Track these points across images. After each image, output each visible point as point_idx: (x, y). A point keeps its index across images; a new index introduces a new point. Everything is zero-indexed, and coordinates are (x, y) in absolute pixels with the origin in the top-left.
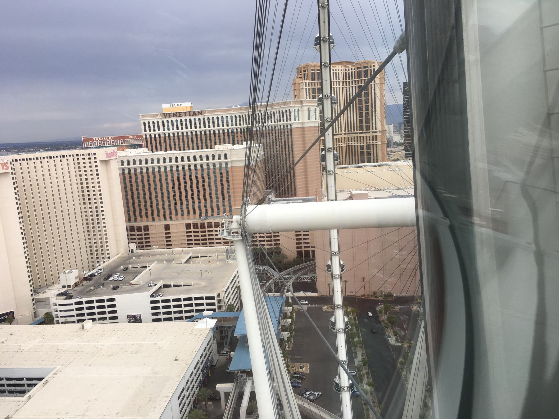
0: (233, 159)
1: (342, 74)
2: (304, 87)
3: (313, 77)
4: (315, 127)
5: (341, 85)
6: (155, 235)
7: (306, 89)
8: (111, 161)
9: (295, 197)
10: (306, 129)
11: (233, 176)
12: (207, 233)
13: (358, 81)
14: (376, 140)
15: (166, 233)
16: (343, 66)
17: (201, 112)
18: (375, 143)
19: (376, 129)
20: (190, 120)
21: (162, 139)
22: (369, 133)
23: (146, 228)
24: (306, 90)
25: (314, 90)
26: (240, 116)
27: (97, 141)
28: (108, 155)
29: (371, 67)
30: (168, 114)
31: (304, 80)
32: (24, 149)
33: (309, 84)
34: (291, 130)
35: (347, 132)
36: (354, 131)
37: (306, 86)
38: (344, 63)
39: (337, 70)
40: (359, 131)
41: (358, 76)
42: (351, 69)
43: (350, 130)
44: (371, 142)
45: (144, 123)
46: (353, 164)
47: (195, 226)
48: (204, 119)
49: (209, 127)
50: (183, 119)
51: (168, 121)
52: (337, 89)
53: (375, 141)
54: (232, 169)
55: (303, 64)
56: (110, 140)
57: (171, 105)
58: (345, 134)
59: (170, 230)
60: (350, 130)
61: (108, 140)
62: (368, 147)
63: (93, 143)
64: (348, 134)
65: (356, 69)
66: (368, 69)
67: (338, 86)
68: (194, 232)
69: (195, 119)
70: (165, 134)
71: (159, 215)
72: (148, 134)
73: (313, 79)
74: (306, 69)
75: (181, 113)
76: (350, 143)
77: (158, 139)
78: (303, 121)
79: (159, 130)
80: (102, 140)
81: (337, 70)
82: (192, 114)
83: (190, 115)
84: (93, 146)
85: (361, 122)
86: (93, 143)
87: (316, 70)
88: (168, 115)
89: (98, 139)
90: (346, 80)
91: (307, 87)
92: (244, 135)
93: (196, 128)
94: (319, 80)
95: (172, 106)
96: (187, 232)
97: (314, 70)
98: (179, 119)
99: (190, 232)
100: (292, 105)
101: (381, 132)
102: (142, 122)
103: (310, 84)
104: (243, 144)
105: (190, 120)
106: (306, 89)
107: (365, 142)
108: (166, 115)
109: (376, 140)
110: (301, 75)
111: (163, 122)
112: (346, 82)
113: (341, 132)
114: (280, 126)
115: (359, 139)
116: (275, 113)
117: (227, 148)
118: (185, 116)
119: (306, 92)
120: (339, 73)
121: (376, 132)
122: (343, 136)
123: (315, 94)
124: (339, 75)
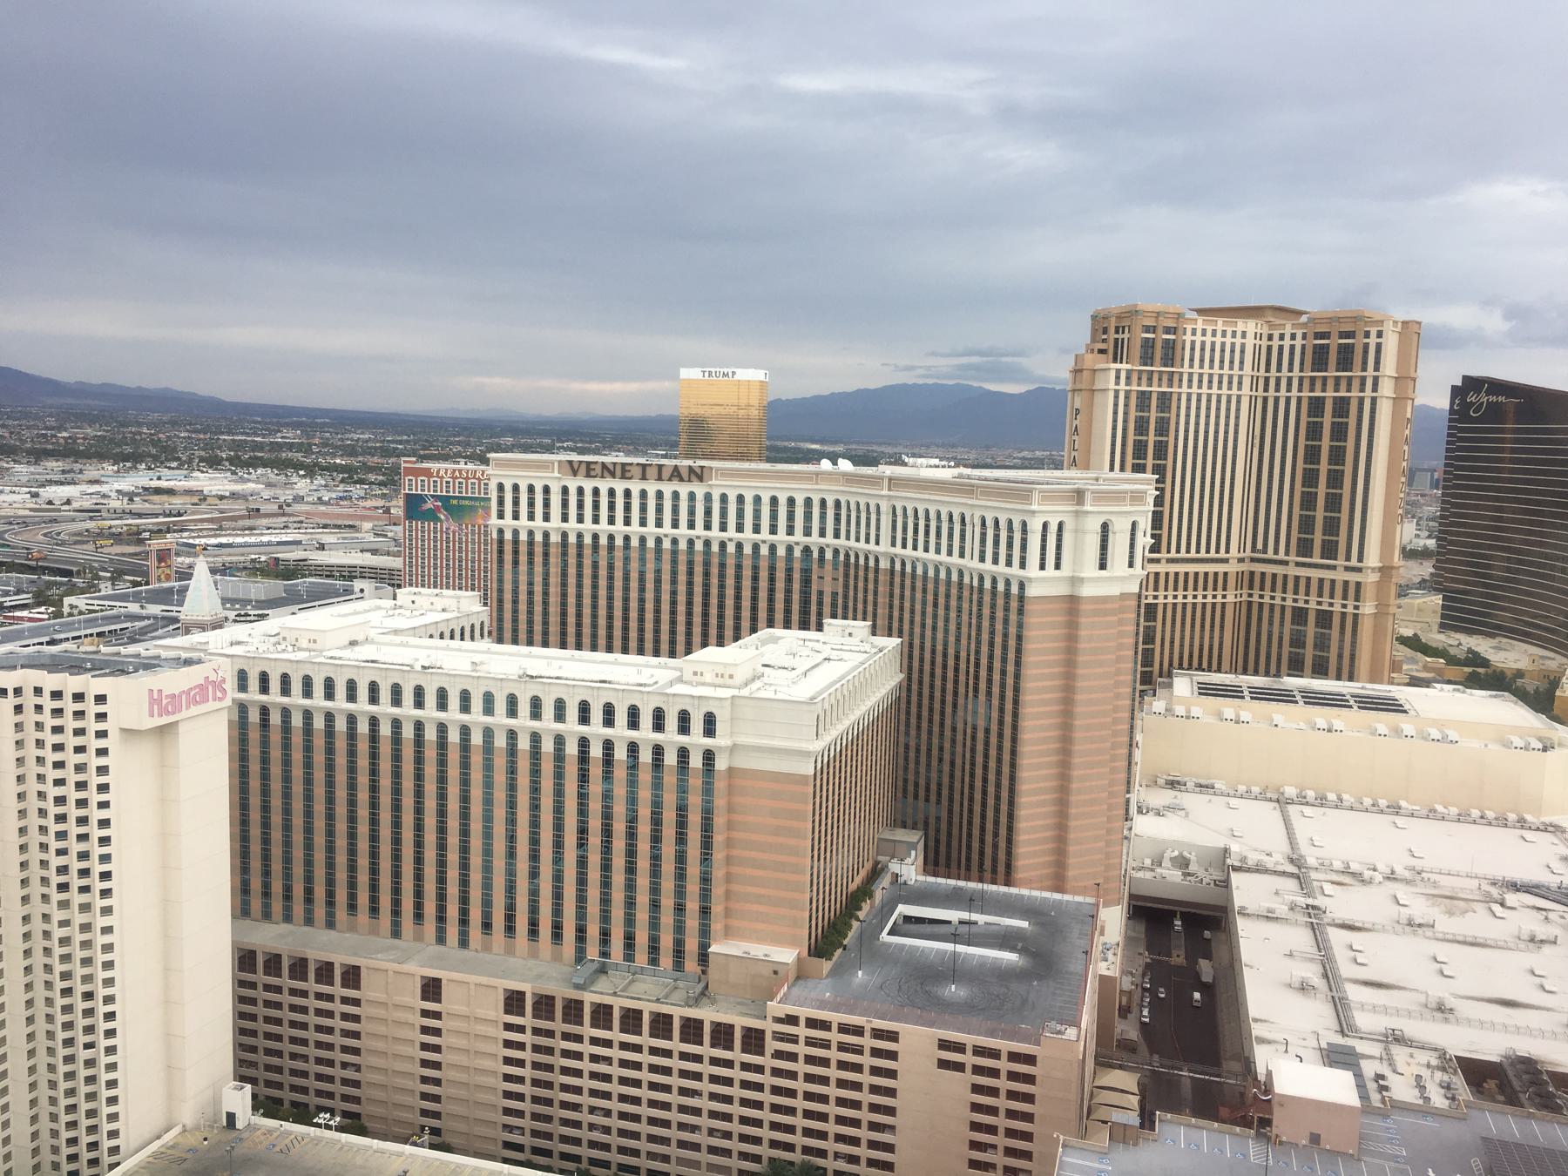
0: (742, 740)
1: (1257, 350)
2: (1112, 386)
3: (1146, 353)
4: (1124, 596)
5: (1246, 390)
6: (381, 1013)
7: (1117, 392)
8: (182, 728)
9: (1008, 883)
10: (1083, 607)
11: (730, 809)
12: (587, 1049)
13: (1313, 379)
14: (1357, 599)
15: (425, 1013)
16: (1260, 322)
17: (699, 471)
18: (1350, 609)
19: (1360, 560)
20: (660, 495)
21: (552, 550)
22: (1334, 568)
23: (352, 976)
24: (1116, 397)
25: (1144, 398)
26: (838, 504)
27: (443, 477)
28: (157, 702)
29: (1367, 335)
30: (583, 467)
31: (1115, 361)
32: (350, 432)
33: (1128, 378)
34: (1021, 598)
35: (1248, 552)
36: (1276, 552)
37: (1117, 383)
38: (1270, 312)
39: (1239, 335)
40: (1293, 558)
41: (1313, 364)
42: (1292, 336)
43: (1260, 546)
44: (1338, 602)
45: (501, 487)
46: (1256, 673)
47: (544, 1005)
48: (708, 497)
49: (723, 528)
50: (636, 487)
51: (580, 491)
52: (1229, 402)
53: (1351, 603)
54: (730, 777)
55: (1115, 304)
56: (479, 479)
57: (704, 372)
58: (1241, 560)
59: (439, 1001)
60: (1260, 546)
61: (474, 478)
62: (1324, 618)
63: (429, 481)
64: (1253, 560)
65: (1310, 336)
66: (1359, 342)
67: (1235, 391)
68: (536, 1032)
69: (676, 495)
70: (565, 535)
71: (419, 916)
72: (508, 526)
73: (1147, 359)
74: (1126, 323)
75: (628, 468)
76: (1256, 592)
77: (538, 550)
78: (1077, 574)
79: (546, 518)
80: (457, 478)
81: (1239, 335)
82: (666, 473)
83: (660, 478)
84: (429, 491)
85: (1307, 525)
86: (429, 481)
87: (1160, 330)
88: (583, 469)
89: (446, 473)
90: (1267, 370)
91: (1122, 386)
92: (846, 576)
93: (675, 525)
94: (1165, 366)
95: (707, 374)
96: (509, 1027)
97: (1153, 329)
98: (620, 486)
99: (521, 1029)
100: (1034, 507)
101: (1380, 569)
102: (493, 486)
103: (1135, 377)
104: (825, 627)
105: (660, 495)
106: (1117, 392)
107: (1313, 599)
108: (576, 467)
109: (1357, 599)
110: (1104, 341)
111: (565, 490)
112: (1267, 380)
113: (1227, 551)
114: (981, 578)
115: (1290, 585)
116: (968, 520)
117: (731, 677)
118: (644, 478)
119: (1116, 405)
120: (1243, 346)
121: (1359, 570)
122: (1232, 568)
123: (1145, 414)
124: (1242, 351)
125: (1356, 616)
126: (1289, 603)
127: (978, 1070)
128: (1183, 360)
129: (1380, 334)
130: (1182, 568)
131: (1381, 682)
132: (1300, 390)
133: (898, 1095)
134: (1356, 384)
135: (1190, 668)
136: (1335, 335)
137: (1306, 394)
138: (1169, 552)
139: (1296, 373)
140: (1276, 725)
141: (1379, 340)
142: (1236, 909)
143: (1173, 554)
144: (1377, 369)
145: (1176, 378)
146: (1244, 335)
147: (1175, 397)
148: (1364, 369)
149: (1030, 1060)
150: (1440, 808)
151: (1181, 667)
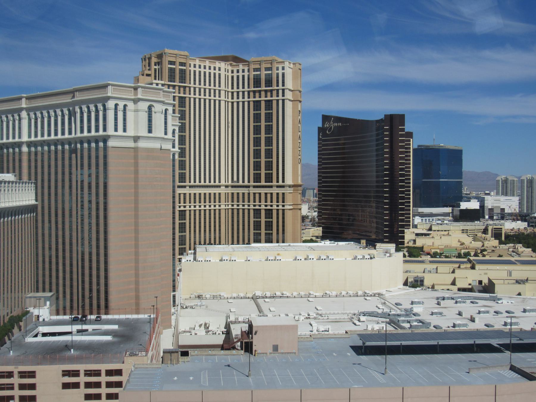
5: (223, 97)
13: (254, 92)
14: (283, 202)
19: (283, 181)
22: (271, 187)
29: (278, 69)
35: (230, 183)
39: (217, 69)
41: (254, 84)
43: (235, 179)
58: (227, 187)
60: (235, 179)
81: (217, 69)
109: (283, 202)
113: (220, 182)
120: (220, 75)
121: (283, 187)
125: (283, 210)
126: (252, 207)
127: (88, 385)
128: (190, 80)
129: (283, 68)
130: (197, 191)
131: (297, 242)
132: (249, 97)
133: (37, 388)
134: (275, 93)
135: (205, 244)
136: (263, 70)
137: (252, 99)
138: (190, 182)
139: (246, 89)
140: (249, 260)
141: (283, 71)
142: (234, 337)
143: (192, 183)
144: (283, 85)
145: (187, 89)
146: (220, 69)
147: (187, 99)
148: (278, 86)
149: (119, 372)
150: (328, 292)
151: (200, 244)
